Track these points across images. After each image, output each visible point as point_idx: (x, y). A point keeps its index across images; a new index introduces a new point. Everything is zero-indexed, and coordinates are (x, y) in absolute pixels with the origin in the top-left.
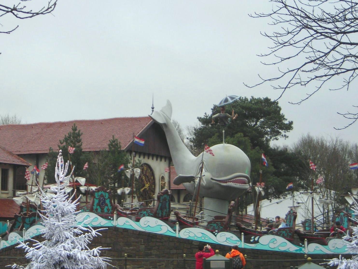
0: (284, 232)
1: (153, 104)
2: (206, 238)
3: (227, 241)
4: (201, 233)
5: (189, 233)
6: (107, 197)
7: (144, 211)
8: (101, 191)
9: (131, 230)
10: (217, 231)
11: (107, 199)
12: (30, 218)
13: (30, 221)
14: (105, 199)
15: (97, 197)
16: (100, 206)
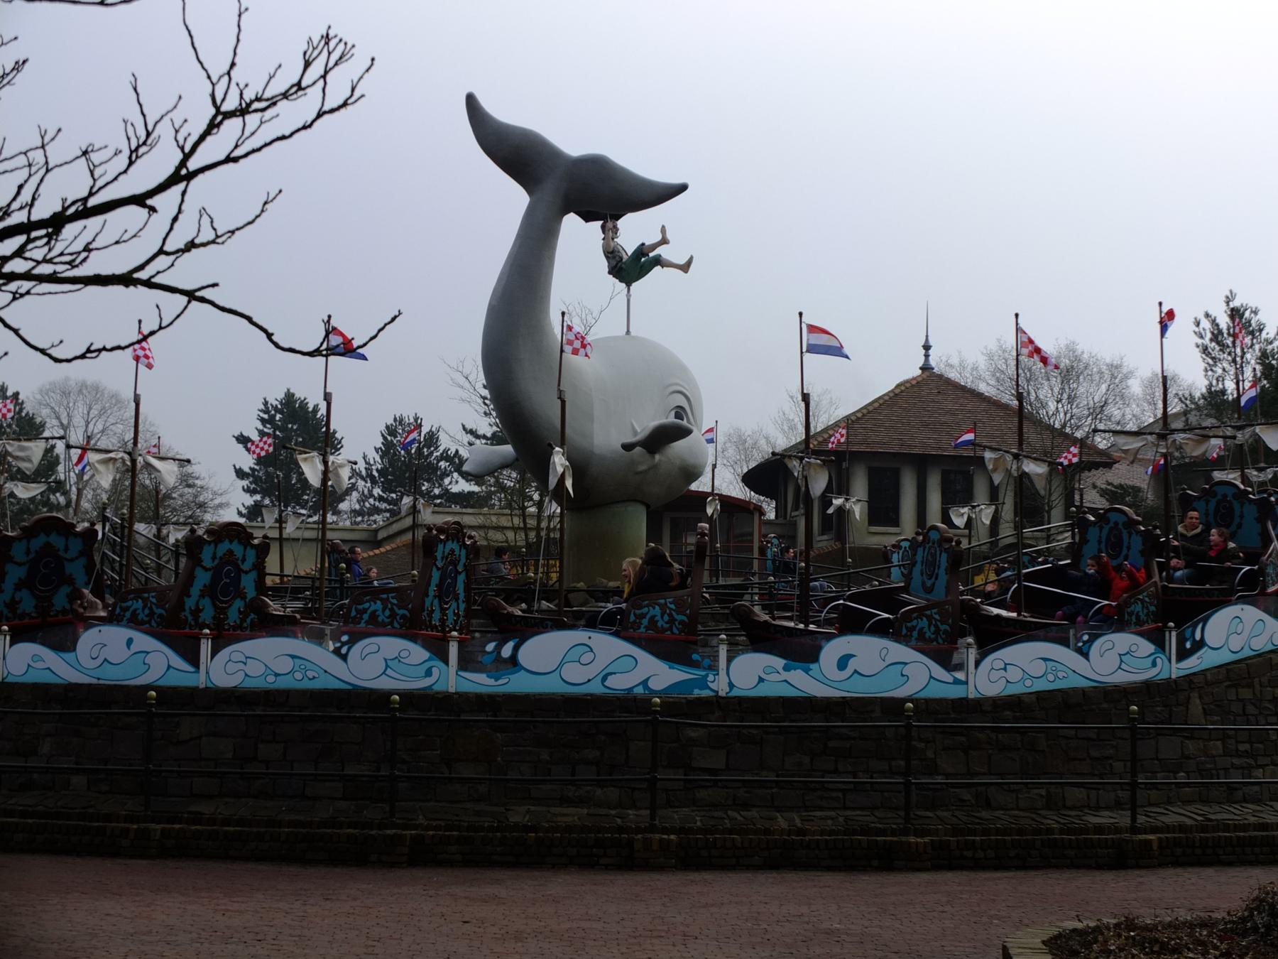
0: (924, 623)
1: (927, 336)
2: (1060, 675)
3: (1124, 666)
4: (1042, 659)
5: (245, 664)
6: (246, 566)
7: (136, 599)
8: (231, 542)
9: (56, 685)
10: (345, 638)
11: (246, 572)
12: (29, 542)
13: (28, 552)
14: (239, 571)
15: (208, 562)
16: (214, 599)
